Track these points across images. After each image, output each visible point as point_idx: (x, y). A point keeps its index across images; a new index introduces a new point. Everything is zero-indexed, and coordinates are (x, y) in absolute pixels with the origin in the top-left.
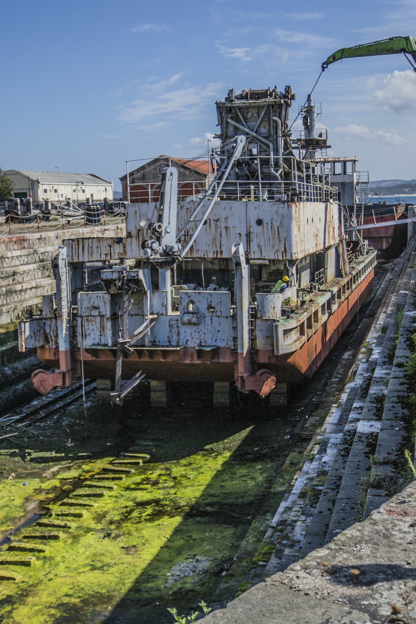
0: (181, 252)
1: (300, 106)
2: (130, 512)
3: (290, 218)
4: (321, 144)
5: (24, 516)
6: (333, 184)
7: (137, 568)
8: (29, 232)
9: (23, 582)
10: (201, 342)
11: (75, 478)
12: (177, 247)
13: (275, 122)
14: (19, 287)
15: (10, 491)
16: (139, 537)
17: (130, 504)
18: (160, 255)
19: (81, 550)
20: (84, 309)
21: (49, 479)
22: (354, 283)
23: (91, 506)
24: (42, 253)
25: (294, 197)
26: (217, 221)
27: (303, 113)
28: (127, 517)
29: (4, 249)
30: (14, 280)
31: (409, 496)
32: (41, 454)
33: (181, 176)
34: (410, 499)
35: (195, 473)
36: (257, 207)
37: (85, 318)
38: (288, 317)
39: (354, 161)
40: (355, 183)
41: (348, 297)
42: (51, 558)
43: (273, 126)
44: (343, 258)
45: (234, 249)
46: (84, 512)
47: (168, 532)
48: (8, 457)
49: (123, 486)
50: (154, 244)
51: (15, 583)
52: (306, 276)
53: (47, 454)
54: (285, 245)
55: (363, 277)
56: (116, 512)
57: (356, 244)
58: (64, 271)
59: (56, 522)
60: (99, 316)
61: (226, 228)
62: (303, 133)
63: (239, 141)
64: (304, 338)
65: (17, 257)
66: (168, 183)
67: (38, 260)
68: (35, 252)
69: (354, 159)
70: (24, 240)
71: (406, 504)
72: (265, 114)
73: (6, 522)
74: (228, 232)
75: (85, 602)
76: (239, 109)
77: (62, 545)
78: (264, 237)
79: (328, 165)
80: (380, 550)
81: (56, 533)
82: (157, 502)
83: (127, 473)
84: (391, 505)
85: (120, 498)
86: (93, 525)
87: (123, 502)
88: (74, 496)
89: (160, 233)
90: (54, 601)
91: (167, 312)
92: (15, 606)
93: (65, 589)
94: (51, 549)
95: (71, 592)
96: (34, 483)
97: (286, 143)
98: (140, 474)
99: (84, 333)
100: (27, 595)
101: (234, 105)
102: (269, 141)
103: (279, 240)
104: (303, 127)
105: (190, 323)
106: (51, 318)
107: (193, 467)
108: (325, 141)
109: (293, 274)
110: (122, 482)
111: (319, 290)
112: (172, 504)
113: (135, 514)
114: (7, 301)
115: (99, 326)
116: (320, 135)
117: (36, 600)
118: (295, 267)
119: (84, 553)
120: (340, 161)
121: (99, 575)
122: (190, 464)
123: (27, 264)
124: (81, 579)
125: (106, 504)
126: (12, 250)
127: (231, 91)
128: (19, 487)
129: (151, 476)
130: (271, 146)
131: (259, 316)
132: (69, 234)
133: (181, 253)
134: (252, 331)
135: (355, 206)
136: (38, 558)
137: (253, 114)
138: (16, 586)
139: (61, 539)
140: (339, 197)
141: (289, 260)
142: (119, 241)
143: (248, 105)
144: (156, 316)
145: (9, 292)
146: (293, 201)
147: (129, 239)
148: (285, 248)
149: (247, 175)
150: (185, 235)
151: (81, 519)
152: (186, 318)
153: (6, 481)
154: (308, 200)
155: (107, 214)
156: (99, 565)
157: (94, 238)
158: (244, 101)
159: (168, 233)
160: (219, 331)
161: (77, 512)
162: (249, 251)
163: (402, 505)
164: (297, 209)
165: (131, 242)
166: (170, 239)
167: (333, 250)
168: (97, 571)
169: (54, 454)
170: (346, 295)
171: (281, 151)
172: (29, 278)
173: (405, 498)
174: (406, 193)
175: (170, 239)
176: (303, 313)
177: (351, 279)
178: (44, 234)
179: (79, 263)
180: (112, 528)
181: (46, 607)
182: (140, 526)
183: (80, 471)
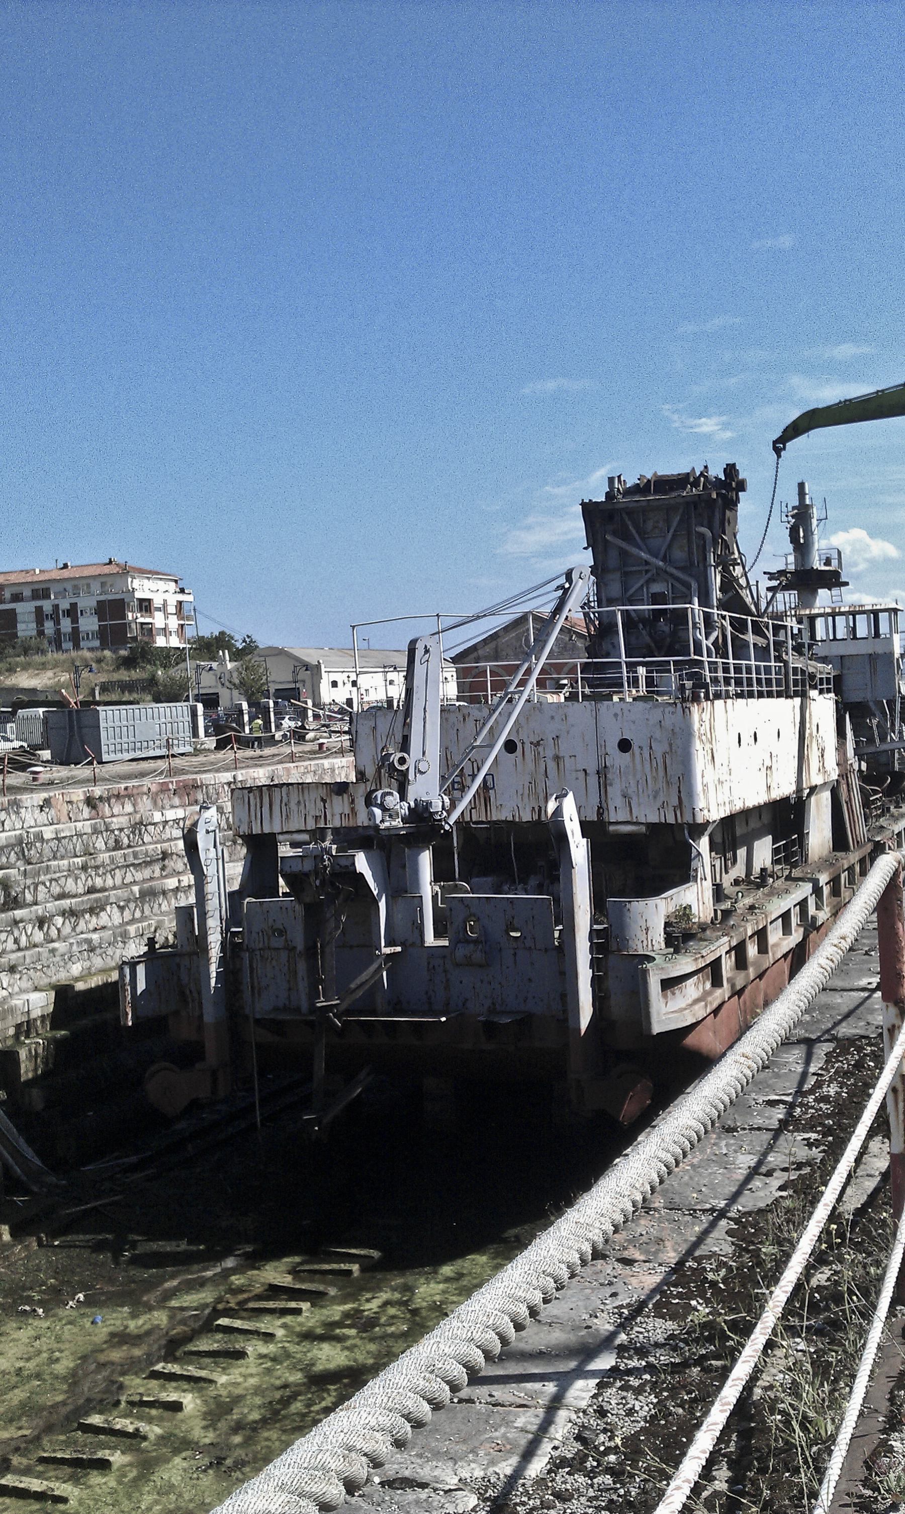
0: (449, 813)
1: (784, 505)
2: (286, 1402)
6: (824, 660)
10: (493, 1004)
13: (702, 536)
15: (58, 1339)
17: (296, 1377)
18: (404, 820)
20: (254, 935)
23: (211, 1381)
25: (697, 690)
26: (538, 744)
27: (790, 518)
28: (276, 1412)
30: (163, 868)
32: (154, 1246)
36: (620, 713)
37: (258, 953)
38: (677, 951)
39: (895, 611)
40: (897, 655)
43: (698, 546)
45: (551, 806)
48: (86, 1254)
49: (298, 1329)
53: (169, 1247)
54: (679, 792)
56: (258, 1401)
60: (285, 948)
61: (557, 758)
62: (791, 559)
64: (723, 992)
69: (893, 606)
72: (681, 521)
74: (561, 766)
76: (628, 514)
77: (113, 1484)
78: (634, 775)
83: (316, 1298)
85: (281, 1363)
88: (185, 1353)
89: (405, 774)
91: (422, 940)
98: (344, 1300)
99: (256, 984)
101: (617, 506)
102: (691, 575)
103: (668, 782)
104: (791, 547)
105: (469, 963)
107: (465, 1283)
108: (836, 574)
110: (300, 1319)
113: (297, 1406)
114: (143, 912)
116: (828, 562)
120: (863, 612)
126: (168, 807)
128: (82, 1327)
129: (368, 1306)
130: (694, 585)
131: (614, 948)
134: (596, 982)
137: (657, 522)
139: (115, 1467)
140: (837, 685)
141: (688, 824)
142: (341, 788)
143: (644, 504)
144: (399, 949)
146: (696, 699)
148: (680, 798)
149: (648, 647)
151: (180, 1415)
152: (461, 952)
154: (739, 696)
157: (292, 784)
159: (422, 773)
160: (530, 980)
161: (173, 1397)
162: (604, 806)
164: (706, 716)
167: (826, 795)
169: (183, 1246)
171: (716, 594)
175: (426, 788)
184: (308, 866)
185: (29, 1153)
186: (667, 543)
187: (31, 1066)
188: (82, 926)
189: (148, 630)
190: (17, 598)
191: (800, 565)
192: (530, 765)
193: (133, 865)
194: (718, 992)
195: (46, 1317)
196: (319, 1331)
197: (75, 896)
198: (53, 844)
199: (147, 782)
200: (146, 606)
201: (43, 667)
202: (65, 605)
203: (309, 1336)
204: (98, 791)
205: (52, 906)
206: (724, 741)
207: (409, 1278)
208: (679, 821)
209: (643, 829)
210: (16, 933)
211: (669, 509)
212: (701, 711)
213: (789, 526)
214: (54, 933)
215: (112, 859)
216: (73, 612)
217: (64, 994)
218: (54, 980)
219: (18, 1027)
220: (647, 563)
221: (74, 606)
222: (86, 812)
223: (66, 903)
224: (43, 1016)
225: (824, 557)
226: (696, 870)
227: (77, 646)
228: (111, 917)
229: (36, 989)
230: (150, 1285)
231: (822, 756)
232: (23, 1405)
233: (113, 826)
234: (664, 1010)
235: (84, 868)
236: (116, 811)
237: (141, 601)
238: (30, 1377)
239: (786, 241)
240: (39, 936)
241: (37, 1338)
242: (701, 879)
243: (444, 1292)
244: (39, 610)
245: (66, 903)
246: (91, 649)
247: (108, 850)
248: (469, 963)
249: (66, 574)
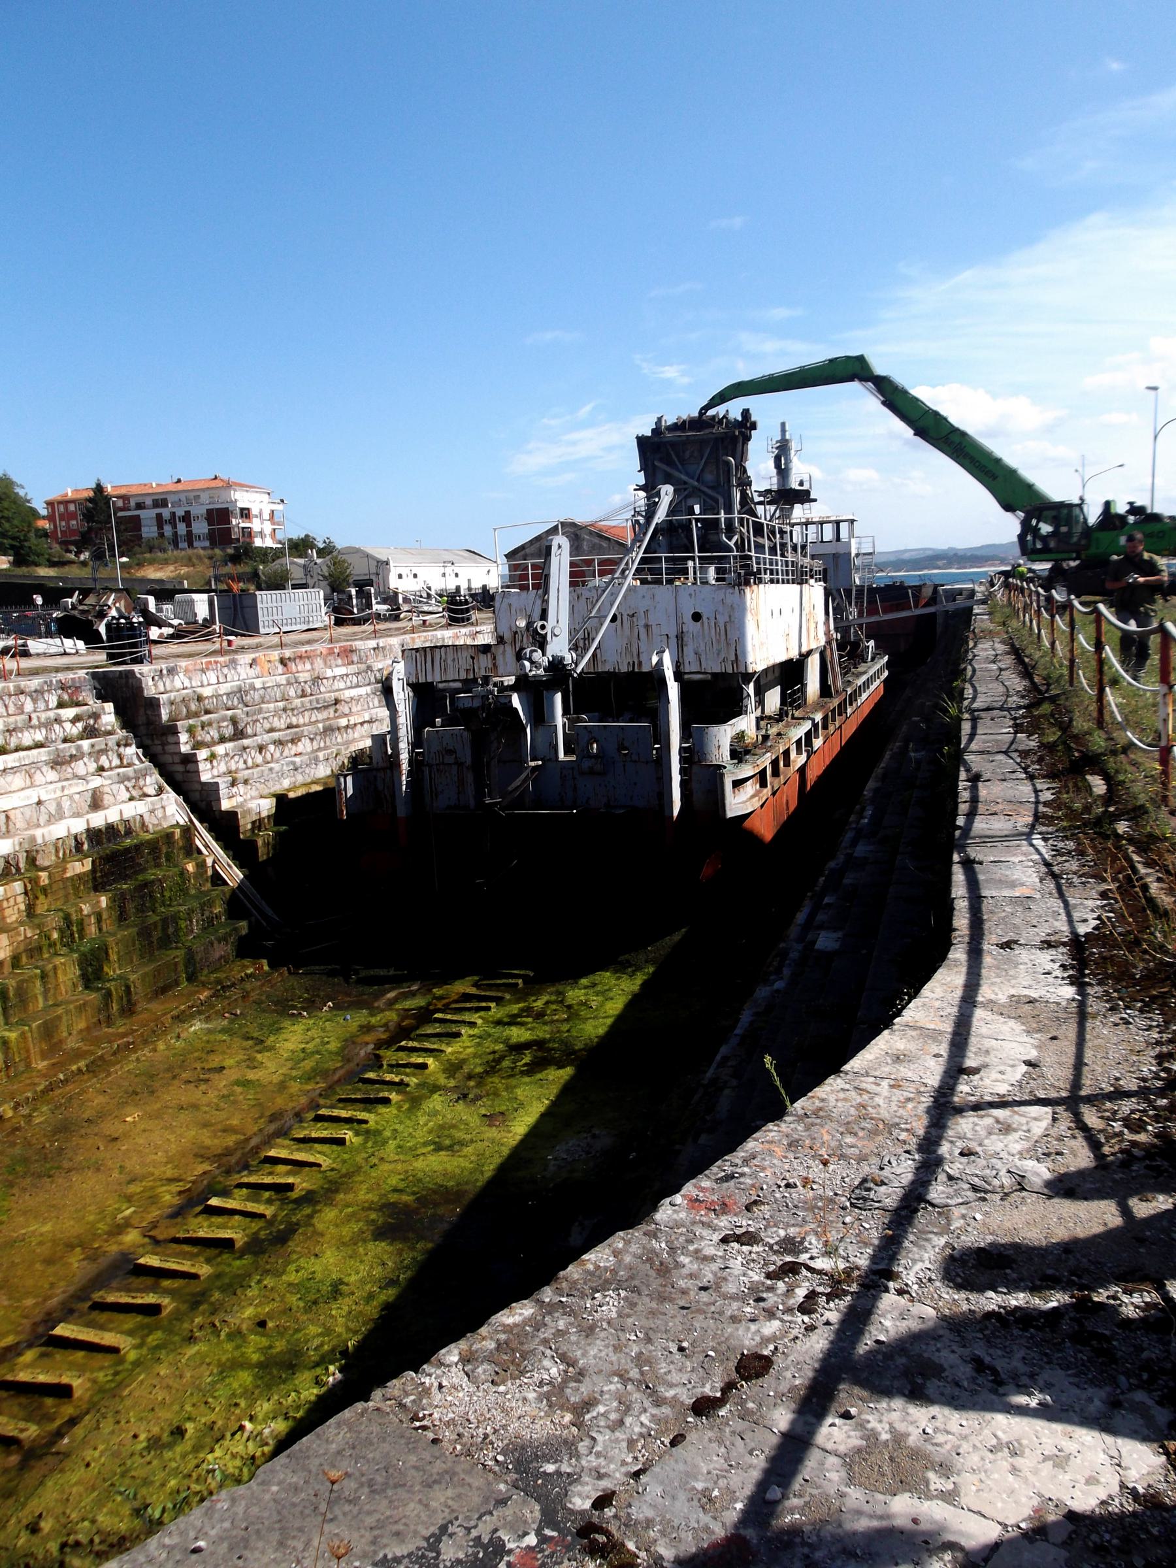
3: (742, 608)
4: (804, 497)
5: (342, 1067)
7: (503, 1148)
8: (361, 639)
9: (332, 1170)
11: (421, 1008)
12: (569, 658)
13: (728, 463)
14: (343, 722)
15: (324, 1030)
16: (509, 1100)
17: (500, 1047)
19: (422, 1121)
21: (383, 1011)
22: (851, 704)
23: (442, 1051)
24: (379, 670)
25: (748, 577)
26: (633, 616)
29: (322, 665)
30: (336, 711)
31: (746, 1162)
33: (576, 549)
34: (746, 1170)
35: (600, 998)
38: (740, 761)
39: (852, 521)
41: (840, 727)
42: (378, 1132)
44: (833, 669)
45: (655, 659)
46: (430, 1061)
47: (553, 1091)
50: (535, 654)
51: (320, 1172)
52: (773, 699)
53: (382, 972)
55: (864, 696)
56: (478, 1061)
57: (856, 645)
58: (402, 696)
59: (389, 1077)
60: (456, 763)
61: (647, 626)
62: (775, 480)
63: (662, 493)
64: (767, 792)
65: (342, 676)
66: (554, 560)
67: (373, 680)
68: (369, 668)
69: (851, 517)
70: (352, 651)
71: (732, 1183)
73: (314, 1077)
75: (422, 1201)
77: (395, 1112)
79: (812, 528)
80: (640, 1307)
81: (386, 1094)
82: (539, 1044)
83: (499, 1001)
84: (706, 1184)
86: (442, 1081)
87: (489, 1045)
90: (376, 1199)
91: (557, 757)
92: (318, 1208)
93: (394, 1181)
94: (378, 1118)
95: (402, 1185)
96: (359, 1018)
97: (744, 496)
100: (337, 1191)
104: (775, 471)
106: (384, 769)
108: (808, 492)
109: (749, 695)
111: (793, 718)
112: (564, 1047)
113: (506, 1063)
115: (456, 779)
116: (801, 484)
117: (350, 1197)
118: (752, 685)
119: (426, 1125)
121: (446, 1159)
122: (594, 985)
123: (358, 686)
124: (419, 1164)
125: (465, 1048)
127: (660, 419)
128: (338, 1023)
130: (721, 501)
132: (420, 640)
133: (576, 666)
134: (683, 784)
135: (854, 589)
136: (357, 1134)
138: (320, 1175)
140: (824, 576)
142: (486, 649)
145: (329, 730)
146: (747, 583)
147: (501, 647)
150: (584, 639)
153: (319, 1014)
154: (772, 581)
155: (479, 610)
156: (448, 1142)
158: (679, 434)
161: (420, 1060)
163: (725, 1185)
165: (504, 651)
166: (559, 646)
168: (443, 1153)
169: (392, 972)
170: (837, 724)
171: (737, 506)
172: (359, 708)
173: (737, 1165)
174: (939, 568)
176: (764, 754)
177: (845, 700)
178: (382, 642)
179: (427, 683)
180: (471, 1084)
181: (363, 1209)
182: (513, 1081)
183: (429, 998)
184: (477, 703)
185: (270, 912)
187: (265, 851)
188: (286, 753)
189: (248, 533)
190: (140, 506)
192: (627, 632)
193: (317, 708)
194: (765, 791)
195: (310, 1017)
196: (506, 1020)
197: (280, 730)
198: (262, 692)
199: (316, 646)
200: (245, 513)
201: (166, 562)
202: (180, 512)
203: (499, 1023)
204: (288, 653)
205: (267, 737)
206: (764, 614)
207: (561, 988)
209: (709, 677)
210: (245, 756)
211: (702, 442)
214: (269, 757)
215: (302, 703)
216: (187, 518)
217: (281, 799)
218: (272, 790)
219: (253, 823)
220: (685, 483)
221: (188, 513)
222: (280, 668)
223: (276, 735)
224: (269, 817)
227: (191, 545)
228: (305, 746)
229: (261, 797)
230: (378, 996)
232: (314, 1070)
233: (301, 680)
234: (734, 802)
235: (285, 710)
236: (300, 668)
237: (242, 509)
238: (313, 1053)
239: (738, 222)
240: (259, 759)
241: (308, 1030)
243: (586, 995)
244: (159, 516)
245: (276, 735)
246: (204, 548)
247: (298, 697)
248: (592, 772)
249: (180, 487)
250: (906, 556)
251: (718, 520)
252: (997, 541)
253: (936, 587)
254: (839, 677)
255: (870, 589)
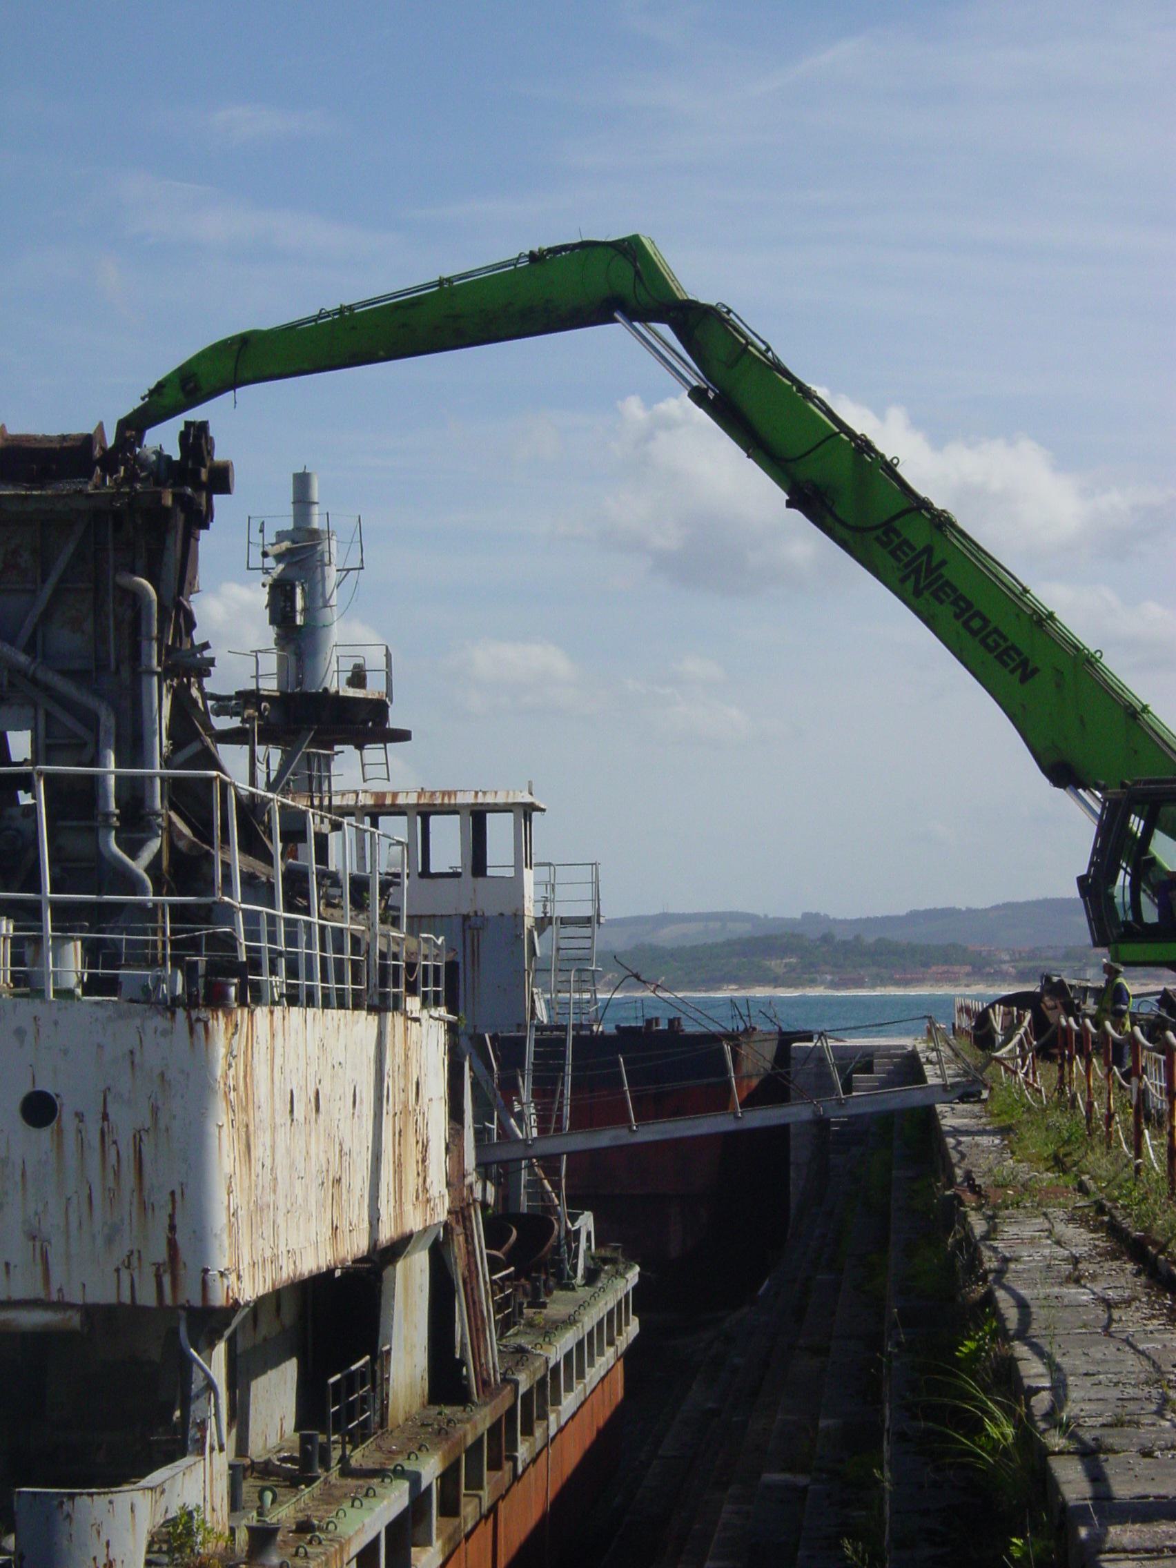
1: (256, 526)
4: (365, 722)
13: (135, 598)
22: (528, 1431)
25: (222, 980)
27: (270, 562)
39: (527, 811)
40: (528, 922)
41: (493, 1509)
44: (473, 1304)
52: (276, 1397)
55: (569, 1402)
62: (270, 663)
97: (183, 708)
104: (271, 632)
108: (379, 708)
109: (210, 1386)
116: (358, 678)
118: (221, 1349)
130: (108, 720)
135: (531, 1036)
140: (450, 988)
141: (190, 1310)
146: (216, 1000)
148: (172, 1245)
154: (292, 999)
164: (239, 1042)
170: (487, 1497)
171: (160, 744)
174: (776, 982)
177: (511, 1412)
186: (41, 606)
191: (292, 679)
208: (168, 1300)
209: (75, 1320)
212: (231, 1030)
213: (268, 580)
225: (348, 665)
226: (202, 1426)
231: (424, 1161)
242: (212, 1449)
250: (666, 937)
251: (94, 782)
252: (962, 899)
253: (786, 1039)
254: (491, 1334)
255: (589, 1045)
